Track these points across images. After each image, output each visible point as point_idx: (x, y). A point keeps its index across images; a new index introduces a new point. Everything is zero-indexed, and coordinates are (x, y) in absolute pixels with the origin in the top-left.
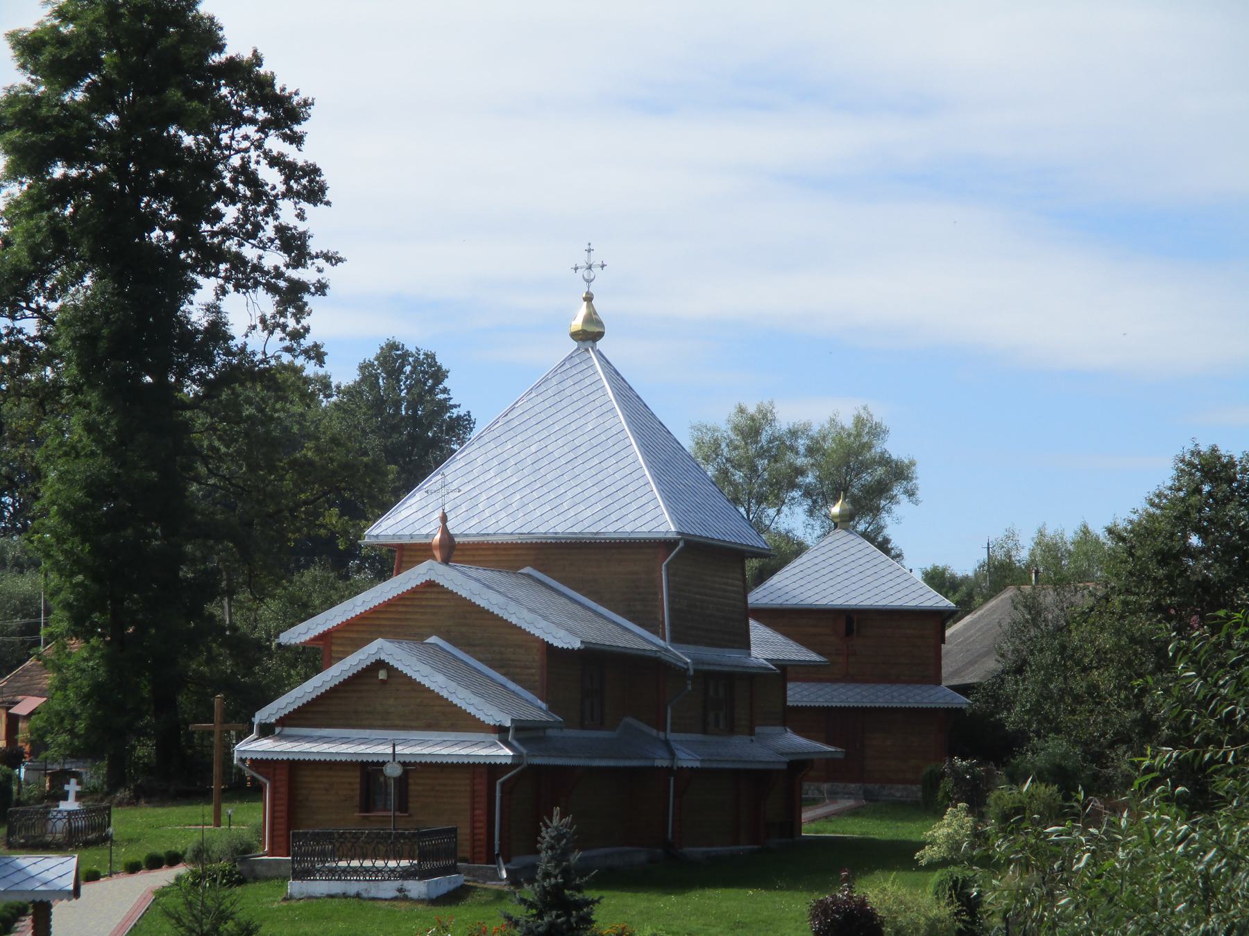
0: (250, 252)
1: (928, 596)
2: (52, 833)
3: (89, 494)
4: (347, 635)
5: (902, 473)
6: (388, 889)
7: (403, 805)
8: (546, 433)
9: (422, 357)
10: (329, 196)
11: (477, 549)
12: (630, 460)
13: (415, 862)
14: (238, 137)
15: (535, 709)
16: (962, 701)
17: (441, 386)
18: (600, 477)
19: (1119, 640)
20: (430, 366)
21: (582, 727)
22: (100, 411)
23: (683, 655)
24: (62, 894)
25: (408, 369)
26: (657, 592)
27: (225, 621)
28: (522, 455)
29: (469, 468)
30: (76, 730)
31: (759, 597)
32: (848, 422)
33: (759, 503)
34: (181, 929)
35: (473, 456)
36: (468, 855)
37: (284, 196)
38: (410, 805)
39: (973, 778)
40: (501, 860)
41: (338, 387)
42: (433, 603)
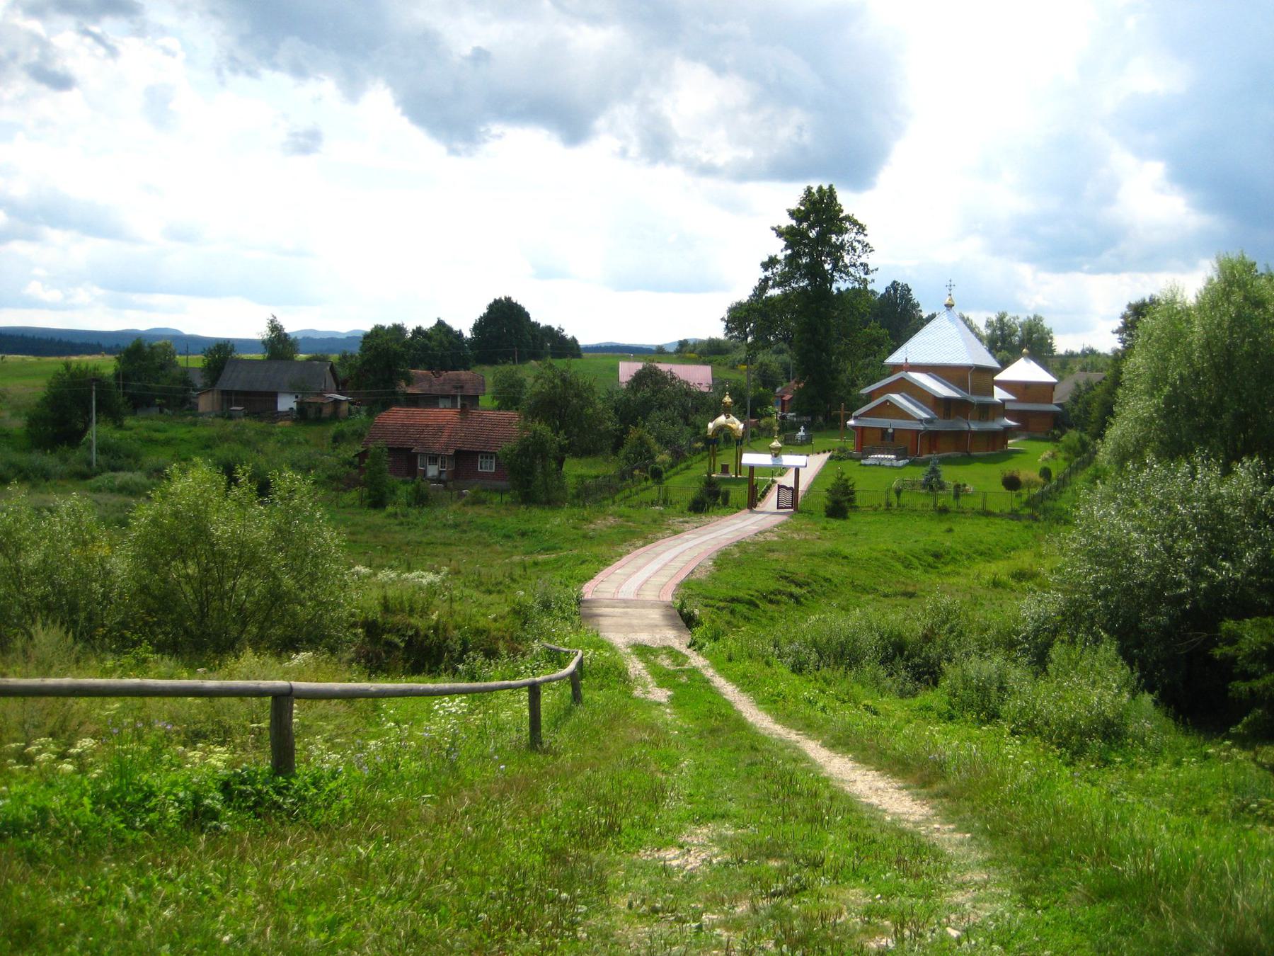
7: (893, 440)
16: (1058, 409)
23: (975, 399)
31: (997, 378)
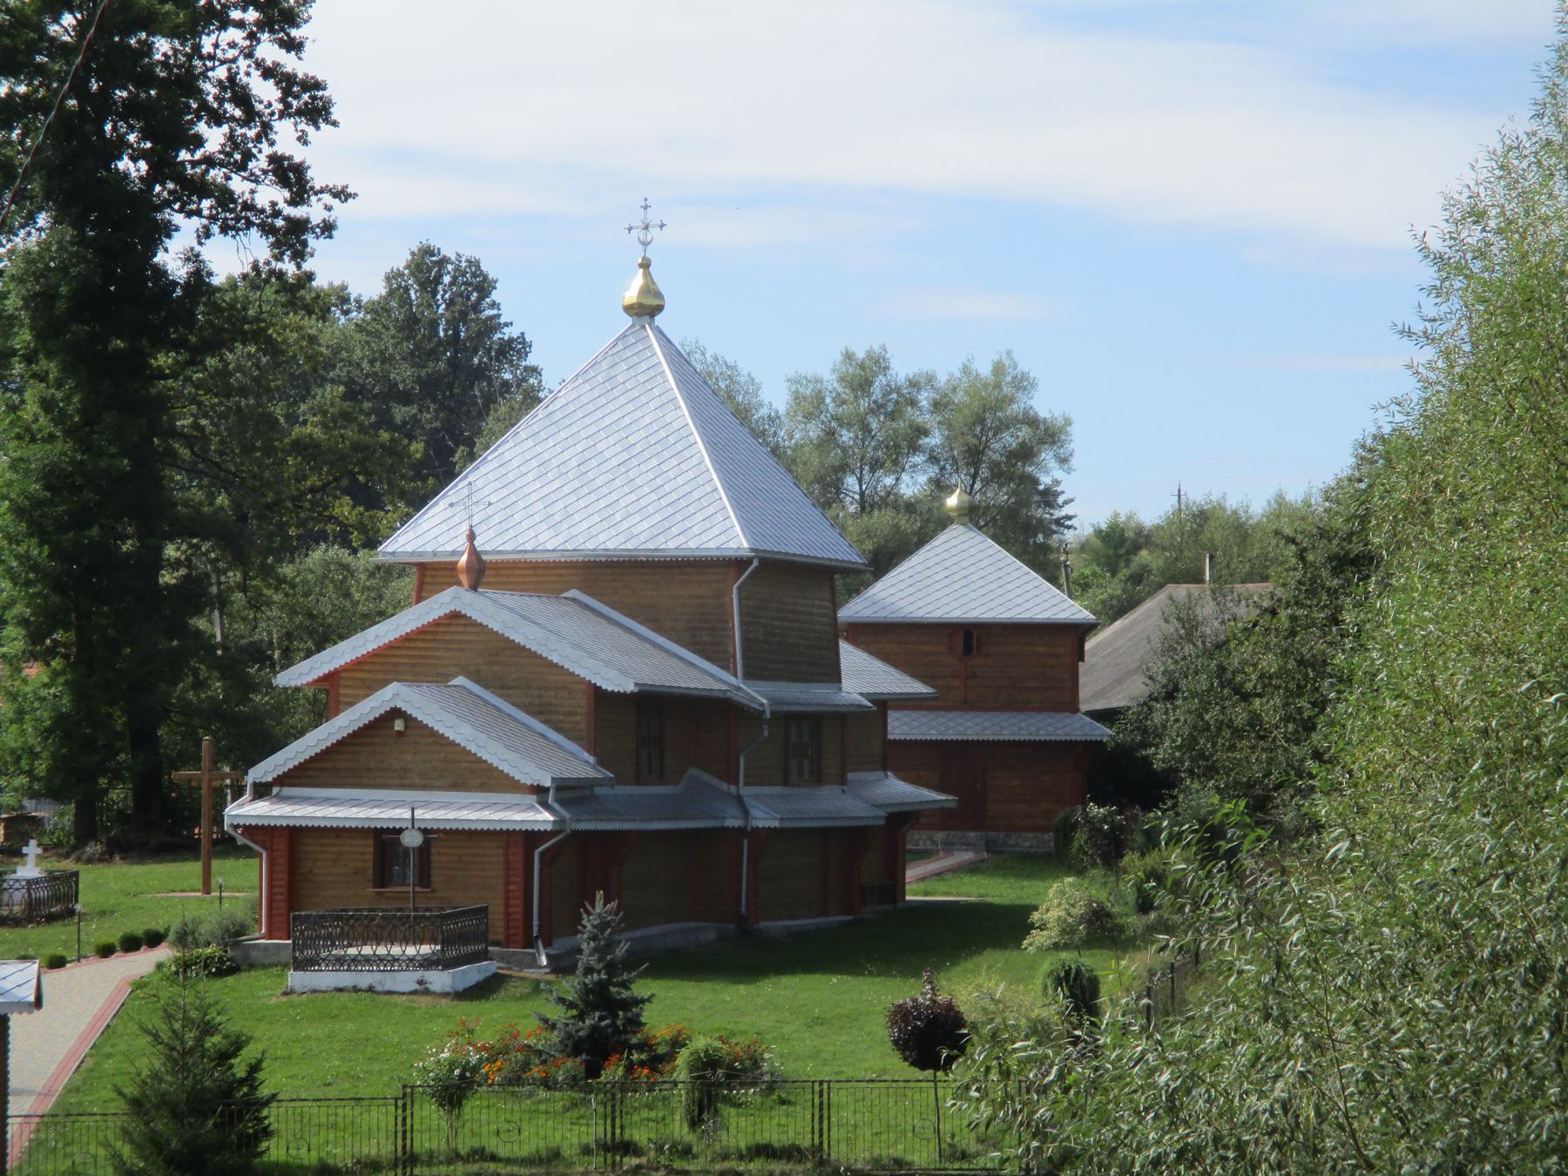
0: (238, 185)
1: (1064, 605)
2: (7, 905)
3: (47, 487)
4: (360, 675)
5: (1052, 435)
6: (406, 980)
7: (424, 879)
8: (594, 428)
9: (463, 264)
10: (335, 113)
11: (512, 569)
12: (695, 461)
13: (438, 947)
14: (223, 45)
15: (580, 764)
16: (1103, 732)
17: (488, 300)
18: (659, 481)
19: (1286, 663)
20: (474, 275)
21: (638, 781)
22: (59, 384)
23: (758, 695)
24: (22, 1006)
25: (447, 279)
26: (726, 619)
27: (214, 636)
28: (566, 455)
29: (502, 471)
30: (36, 772)
31: (855, 609)
32: (984, 369)
33: (873, 470)
34: (160, 1047)
35: (508, 456)
36: (501, 937)
37: (282, 115)
38: (433, 879)
39: (1112, 829)
40: (540, 943)
41: (358, 301)
42: (458, 637)
